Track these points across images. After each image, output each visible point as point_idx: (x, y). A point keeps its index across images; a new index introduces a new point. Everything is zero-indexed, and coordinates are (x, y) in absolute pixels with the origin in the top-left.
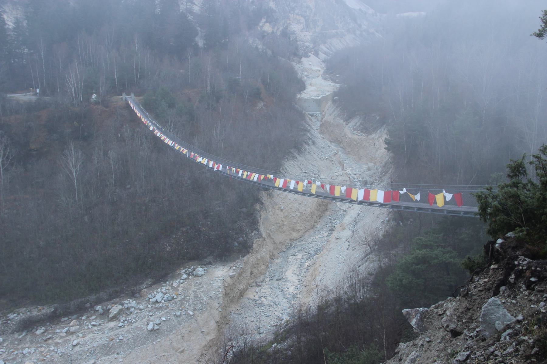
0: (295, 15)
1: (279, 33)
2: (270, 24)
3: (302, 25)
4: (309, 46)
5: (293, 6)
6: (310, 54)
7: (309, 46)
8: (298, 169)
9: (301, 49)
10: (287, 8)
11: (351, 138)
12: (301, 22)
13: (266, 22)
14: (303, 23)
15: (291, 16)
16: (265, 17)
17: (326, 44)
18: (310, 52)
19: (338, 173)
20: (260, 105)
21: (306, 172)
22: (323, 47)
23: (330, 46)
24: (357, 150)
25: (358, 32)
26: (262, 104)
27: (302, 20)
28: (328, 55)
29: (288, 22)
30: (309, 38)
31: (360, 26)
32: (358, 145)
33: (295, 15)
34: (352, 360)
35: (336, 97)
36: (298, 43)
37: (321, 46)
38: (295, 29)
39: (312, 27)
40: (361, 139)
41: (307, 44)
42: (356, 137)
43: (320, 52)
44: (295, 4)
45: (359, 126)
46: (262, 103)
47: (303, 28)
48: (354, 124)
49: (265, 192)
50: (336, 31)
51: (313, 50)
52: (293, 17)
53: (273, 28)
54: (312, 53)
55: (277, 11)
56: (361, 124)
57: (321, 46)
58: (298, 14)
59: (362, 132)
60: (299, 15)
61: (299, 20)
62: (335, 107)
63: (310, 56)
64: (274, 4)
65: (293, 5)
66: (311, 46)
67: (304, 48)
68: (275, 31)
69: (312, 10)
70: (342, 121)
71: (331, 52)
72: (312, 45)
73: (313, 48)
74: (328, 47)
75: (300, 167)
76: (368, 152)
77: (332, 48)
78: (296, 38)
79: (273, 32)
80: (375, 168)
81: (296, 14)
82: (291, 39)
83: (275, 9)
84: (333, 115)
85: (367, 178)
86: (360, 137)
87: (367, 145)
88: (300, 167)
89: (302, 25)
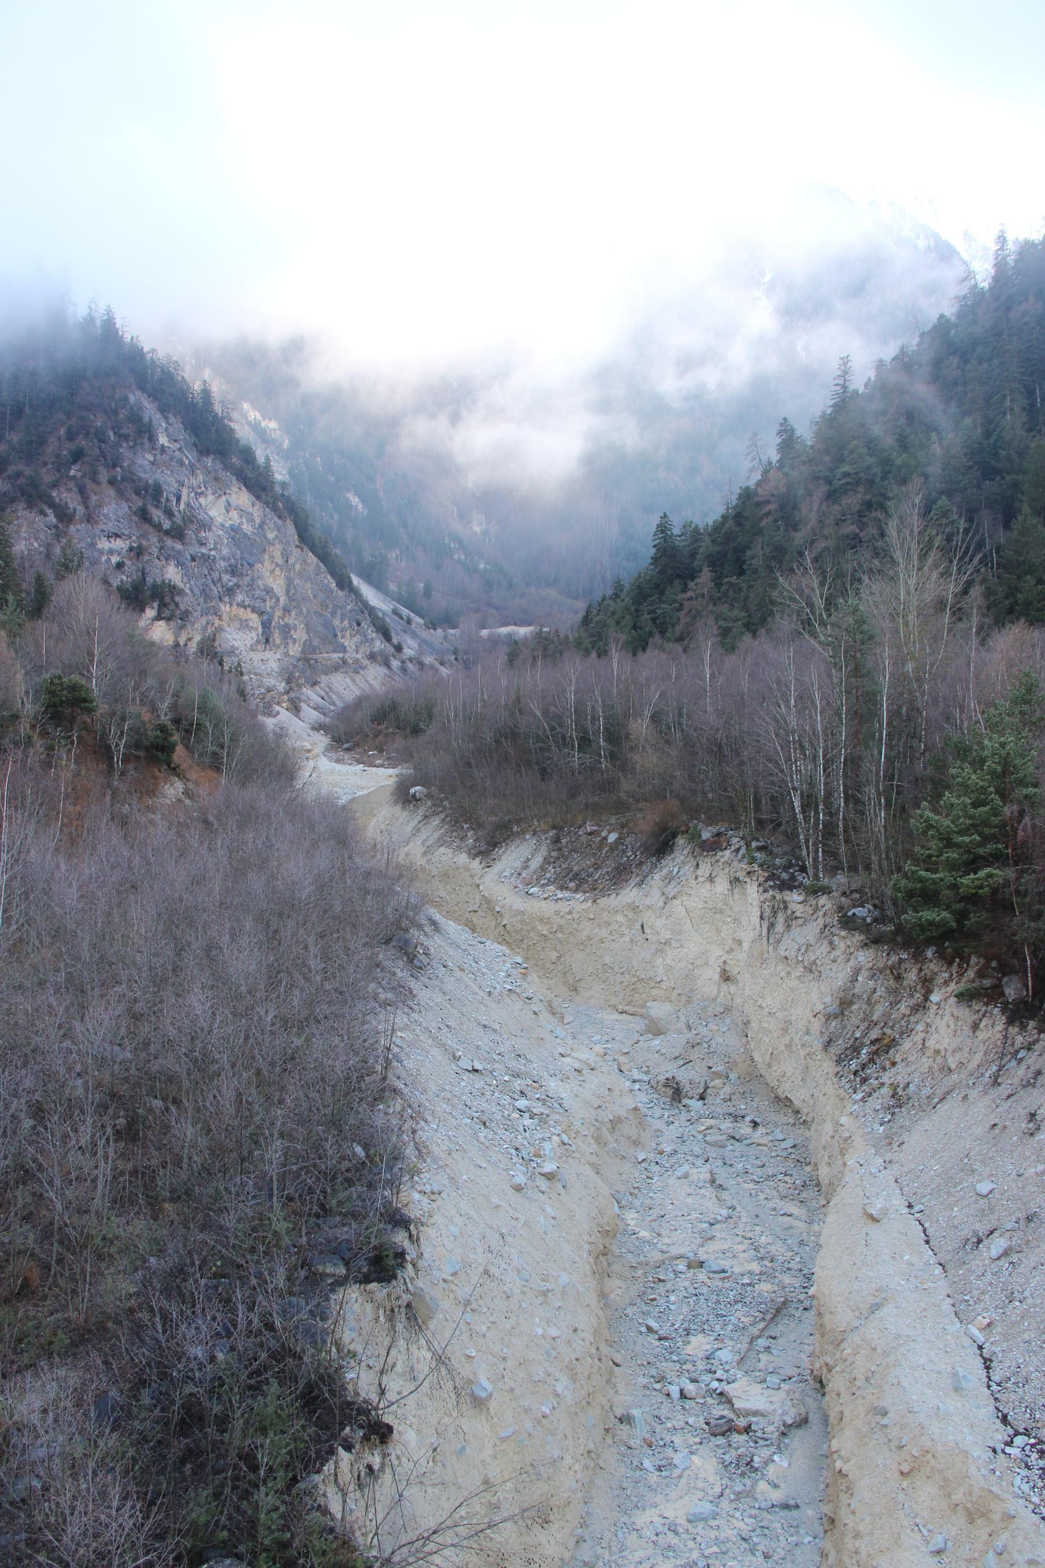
0: (235, 607)
1: (193, 647)
2: (168, 625)
3: (254, 634)
4: (275, 686)
5: (231, 584)
6: (277, 708)
7: (275, 686)
8: (435, 1052)
9: (253, 695)
10: (213, 587)
11: (523, 913)
12: (251, 624)
13: (159, 618)
14: (257, 629)
15: (225, 608)
16: (156, 605)
17: (317, 687)
18: (278, 703)
19: (573, 1054)
20: (172, 790)
21: (478, 1066)
22: (308, 692)
23: (327, 693)
24: (554, 955)
25: (395, 663)
26: (181, 790)
27: (255, 620)
28: (324, 714)
29: (217, 623)
30: (274, 665)
31: (399, 648)
32: (559, 935)
33: (235, 607)
34: (354, 1518)
35: (418, 788)
36: (246, 678)
37: (304, 689)
38: (236, 644)
39: (278, 641)
40: (570, 913)
41: (270, 682)
42: (548, 908)
43: (303, 706)
44: (235, 580)
45: (543, 869)
46: (179, 786)
47: (258, 642)
48: (518, 864)
49: (370, 1297)
50: (341, 655)
51: (286, 697)
52: (231, 611)
53: (177, 636)
54: (284, 705)
55: (187, 591)
56: (547, 861)
57: (304, 689)
58: (242, 605)
59: (562, 888)
60: (245, 608)
61: (246, 620)
62: (419, 818)
63: (278, 713)
64: (178, 573)
65: (230, 581)
66: (282, 686)
67: (263, 691)
68: (182, 643)
69: (278, 600)
70: (463, 858)
71: (333, 708)
72: (283, 684)
73: (287, 692)
74: (323, 694)
75: (442, 1046)
76: (607, 959)
77: (334, 697)
78: (239, 665)
79: (177, 645)
80: (682, 1025)
81: (238, 605)
82: (226, 668)
83: (181, 585)
84: (419, 842)
85: (667, 1070)
86: (560, 906)
87: (604, 933)
88: (442, 1046)
89: (254, 634)
